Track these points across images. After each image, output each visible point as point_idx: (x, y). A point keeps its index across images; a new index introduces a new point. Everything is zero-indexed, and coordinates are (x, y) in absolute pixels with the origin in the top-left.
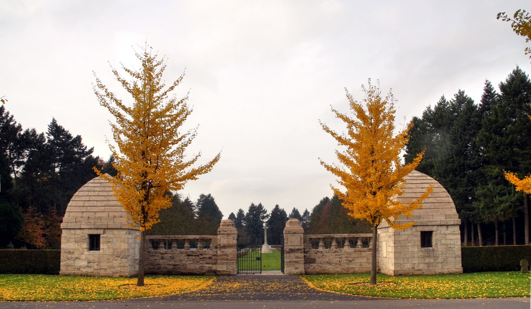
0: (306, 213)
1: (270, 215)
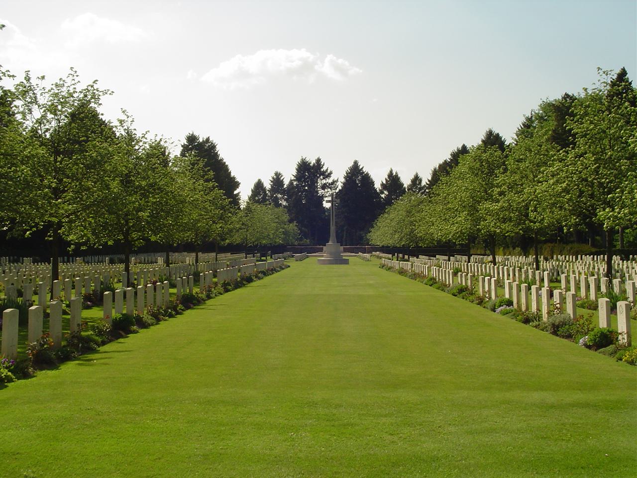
0: (416, 180)
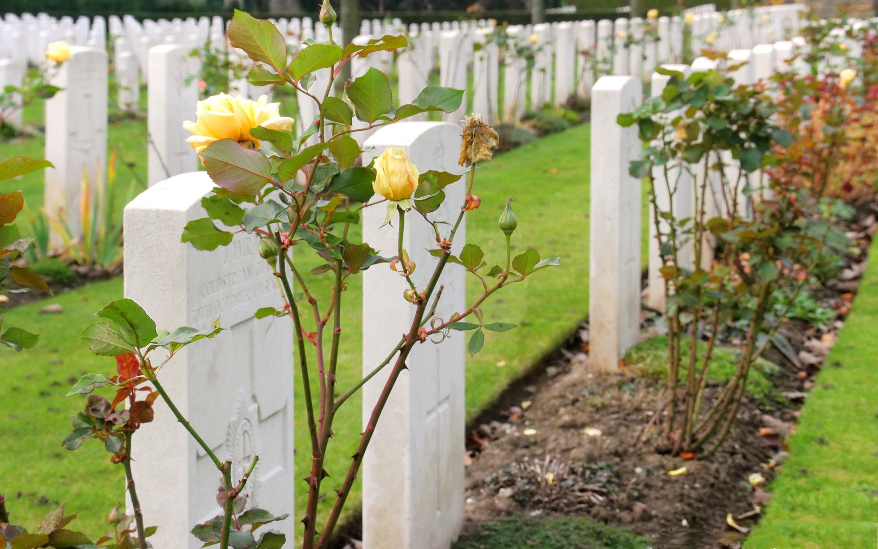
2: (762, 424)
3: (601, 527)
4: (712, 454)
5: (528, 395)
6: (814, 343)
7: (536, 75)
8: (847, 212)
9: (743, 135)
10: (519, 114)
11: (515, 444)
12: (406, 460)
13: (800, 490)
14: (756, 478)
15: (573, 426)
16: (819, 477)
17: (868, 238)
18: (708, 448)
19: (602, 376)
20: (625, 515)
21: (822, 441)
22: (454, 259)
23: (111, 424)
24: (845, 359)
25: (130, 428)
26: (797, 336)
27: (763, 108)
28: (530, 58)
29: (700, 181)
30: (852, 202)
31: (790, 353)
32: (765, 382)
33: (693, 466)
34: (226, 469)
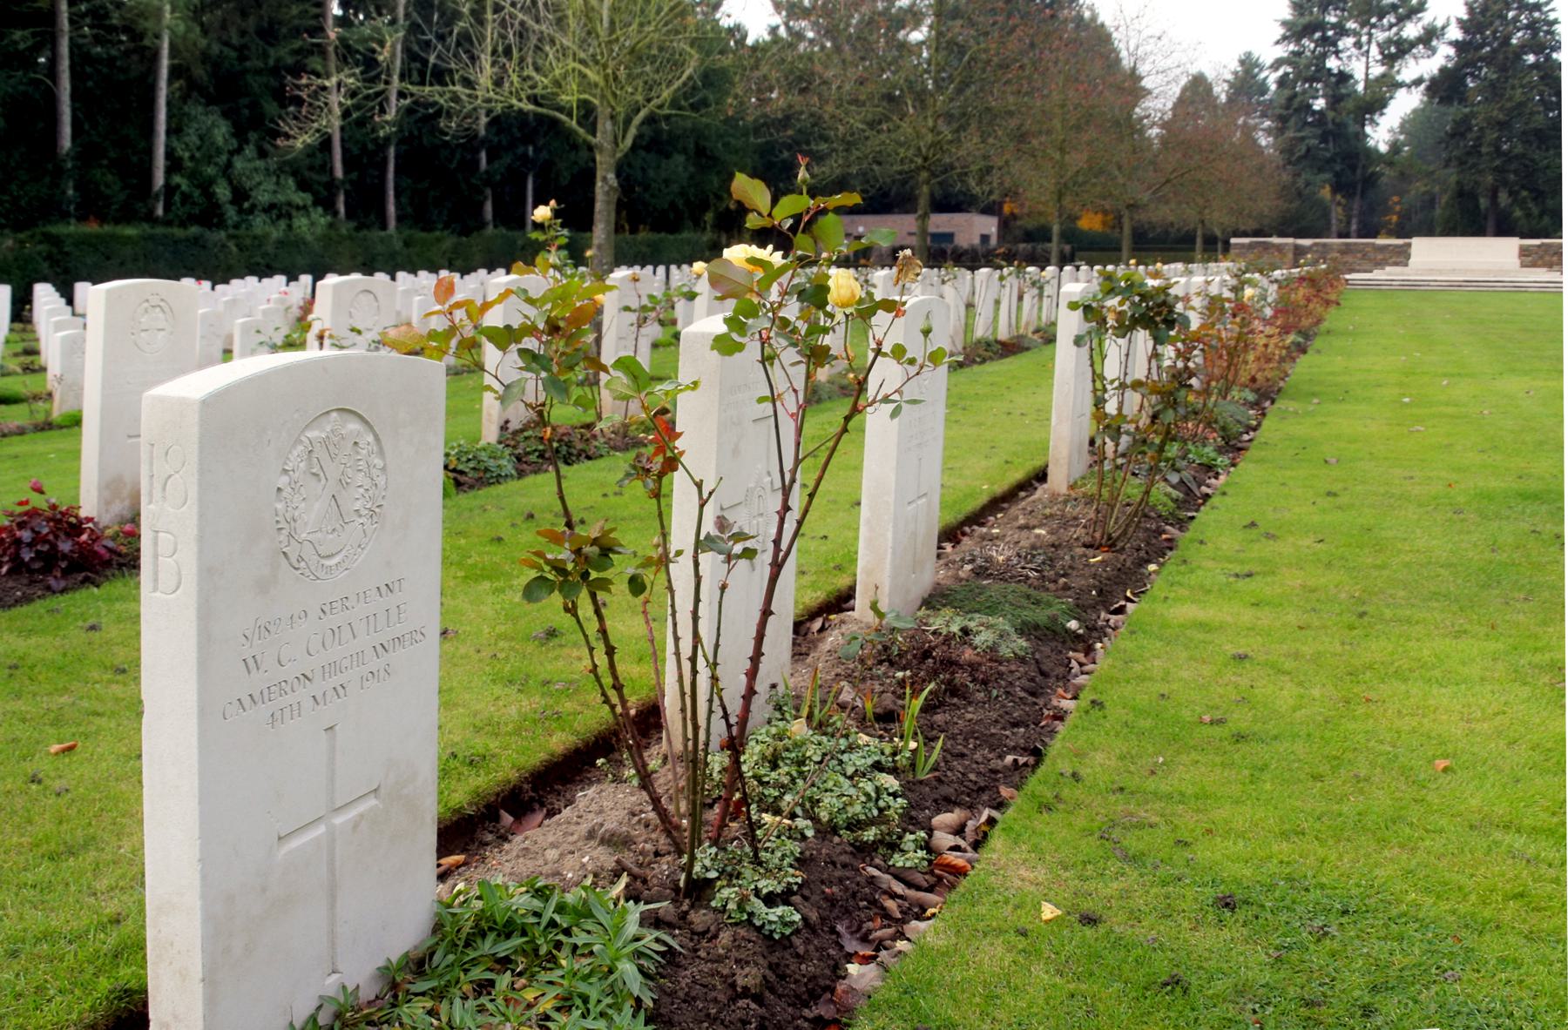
1: (1455, 33)
2: (1164, 532)
3: (1031, 592)
4: (1123, 548)
5: (1002, 510)
6: (1213, 481)
7: (1046, 301)
8: (1251, 397)
9: (1158, 319)
10: (1031, 329)
11: (983, 538)
12: (890, 535)
13: (1179, 572)
14: (1152, 567)
15: (1027, 527)
16: (1194, 565)
17: (1264, 415)
18: (1120, 545)
19: (1054, 497)
20: (1052, 586)
21: (1201, 542)
22: (885, 355)
23: (648, 471)
24: (1229, 491)
25: (661, 475)
26: (1201, 476)
27: (1170, 299)
28: (1041, 288)
29: (1124, 351)
30: (1257, 391)
31: (1194, 487)
32: (1171, 504)
33: (1107, 556)
34: (699, 485)
